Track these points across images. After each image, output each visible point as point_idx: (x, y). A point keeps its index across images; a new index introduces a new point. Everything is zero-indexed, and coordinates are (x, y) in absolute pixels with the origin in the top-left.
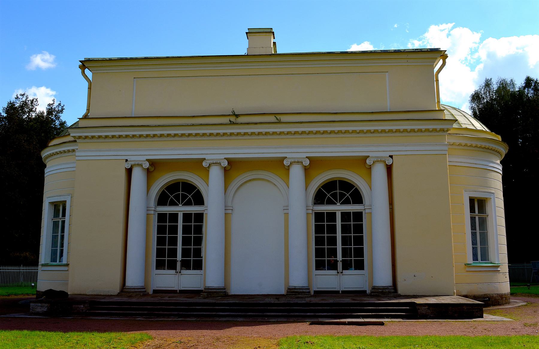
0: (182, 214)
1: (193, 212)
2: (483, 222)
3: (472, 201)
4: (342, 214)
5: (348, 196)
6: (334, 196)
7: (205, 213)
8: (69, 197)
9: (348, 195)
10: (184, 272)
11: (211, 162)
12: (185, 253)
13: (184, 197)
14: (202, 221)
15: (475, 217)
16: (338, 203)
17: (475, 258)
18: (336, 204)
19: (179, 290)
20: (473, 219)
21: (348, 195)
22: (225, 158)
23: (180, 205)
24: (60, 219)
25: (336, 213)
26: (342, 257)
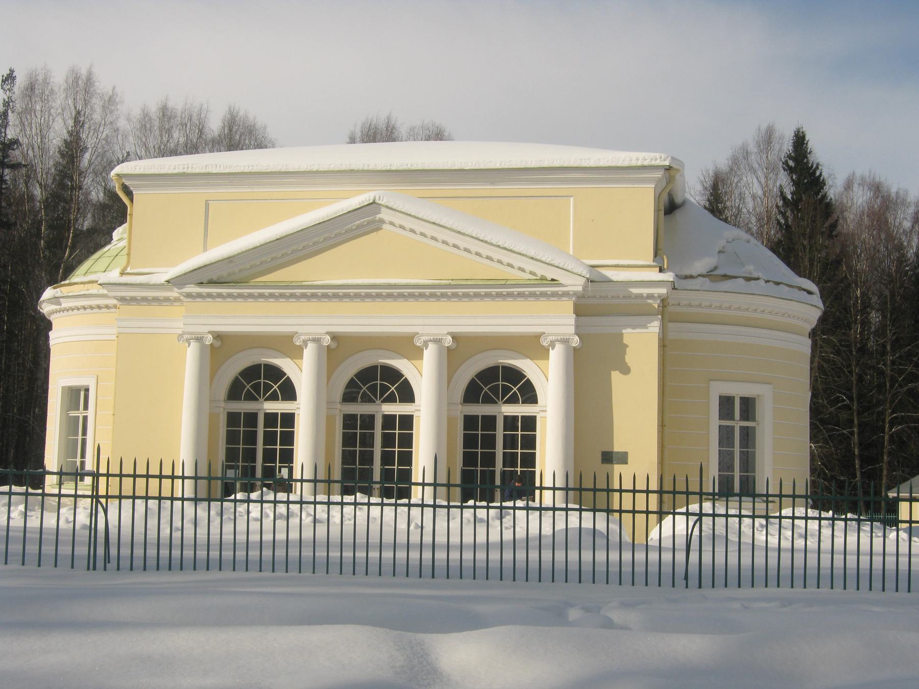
0: (754, 426)
3: (726, 403)
5: (275, 389)
6: (373, 389)
7: (296, 412)
9: (500, 383)
13: (506, 390)
14: (411, 427)
16: (260, 398)
18: (374, 402)
20: (726, 435)
21: (486, 389)
25: (535, 417)
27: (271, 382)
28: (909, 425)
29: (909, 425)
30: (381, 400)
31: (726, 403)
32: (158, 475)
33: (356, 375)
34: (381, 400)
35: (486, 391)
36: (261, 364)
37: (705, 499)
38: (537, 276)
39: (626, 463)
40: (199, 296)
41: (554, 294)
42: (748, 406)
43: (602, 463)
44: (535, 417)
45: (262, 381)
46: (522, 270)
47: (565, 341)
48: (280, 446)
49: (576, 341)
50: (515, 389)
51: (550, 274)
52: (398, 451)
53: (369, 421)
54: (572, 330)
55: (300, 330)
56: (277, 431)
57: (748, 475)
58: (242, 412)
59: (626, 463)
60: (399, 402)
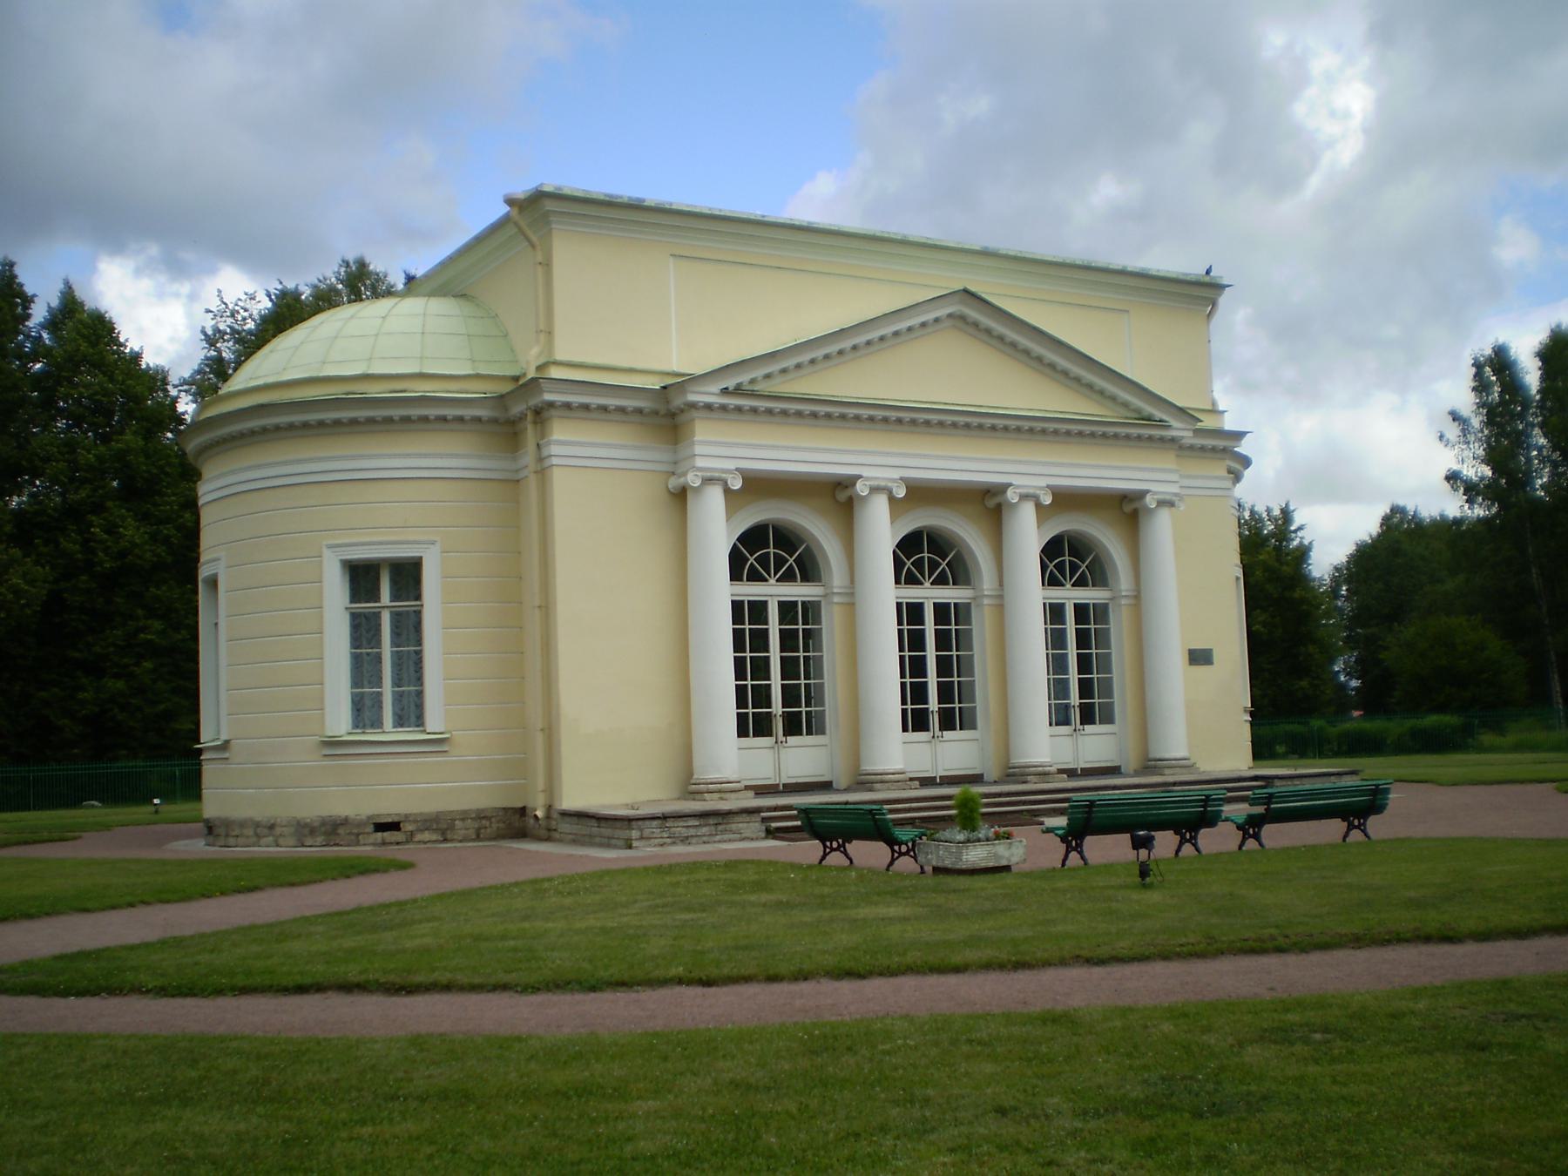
2: (410, 628)
3: (362, 577)
4: (781, 604)
6: (763, 560)
9: (926, 555)
11: (1160, 497)
15: (377, 616)
17: (364, 711)
19: (1081, 769)
20: (363, 629)
23: (772, 581)
25: (766, 602)
30: (931, 581)
31: (362, 577)
34: (777, 576)
40: (723, 408)
41: (1162, 439)
42: (407, 575)
46: (1125, 405)
50: (791, 561)
51: (1158, 414)
52: (909, 651)
55: (865, 472)
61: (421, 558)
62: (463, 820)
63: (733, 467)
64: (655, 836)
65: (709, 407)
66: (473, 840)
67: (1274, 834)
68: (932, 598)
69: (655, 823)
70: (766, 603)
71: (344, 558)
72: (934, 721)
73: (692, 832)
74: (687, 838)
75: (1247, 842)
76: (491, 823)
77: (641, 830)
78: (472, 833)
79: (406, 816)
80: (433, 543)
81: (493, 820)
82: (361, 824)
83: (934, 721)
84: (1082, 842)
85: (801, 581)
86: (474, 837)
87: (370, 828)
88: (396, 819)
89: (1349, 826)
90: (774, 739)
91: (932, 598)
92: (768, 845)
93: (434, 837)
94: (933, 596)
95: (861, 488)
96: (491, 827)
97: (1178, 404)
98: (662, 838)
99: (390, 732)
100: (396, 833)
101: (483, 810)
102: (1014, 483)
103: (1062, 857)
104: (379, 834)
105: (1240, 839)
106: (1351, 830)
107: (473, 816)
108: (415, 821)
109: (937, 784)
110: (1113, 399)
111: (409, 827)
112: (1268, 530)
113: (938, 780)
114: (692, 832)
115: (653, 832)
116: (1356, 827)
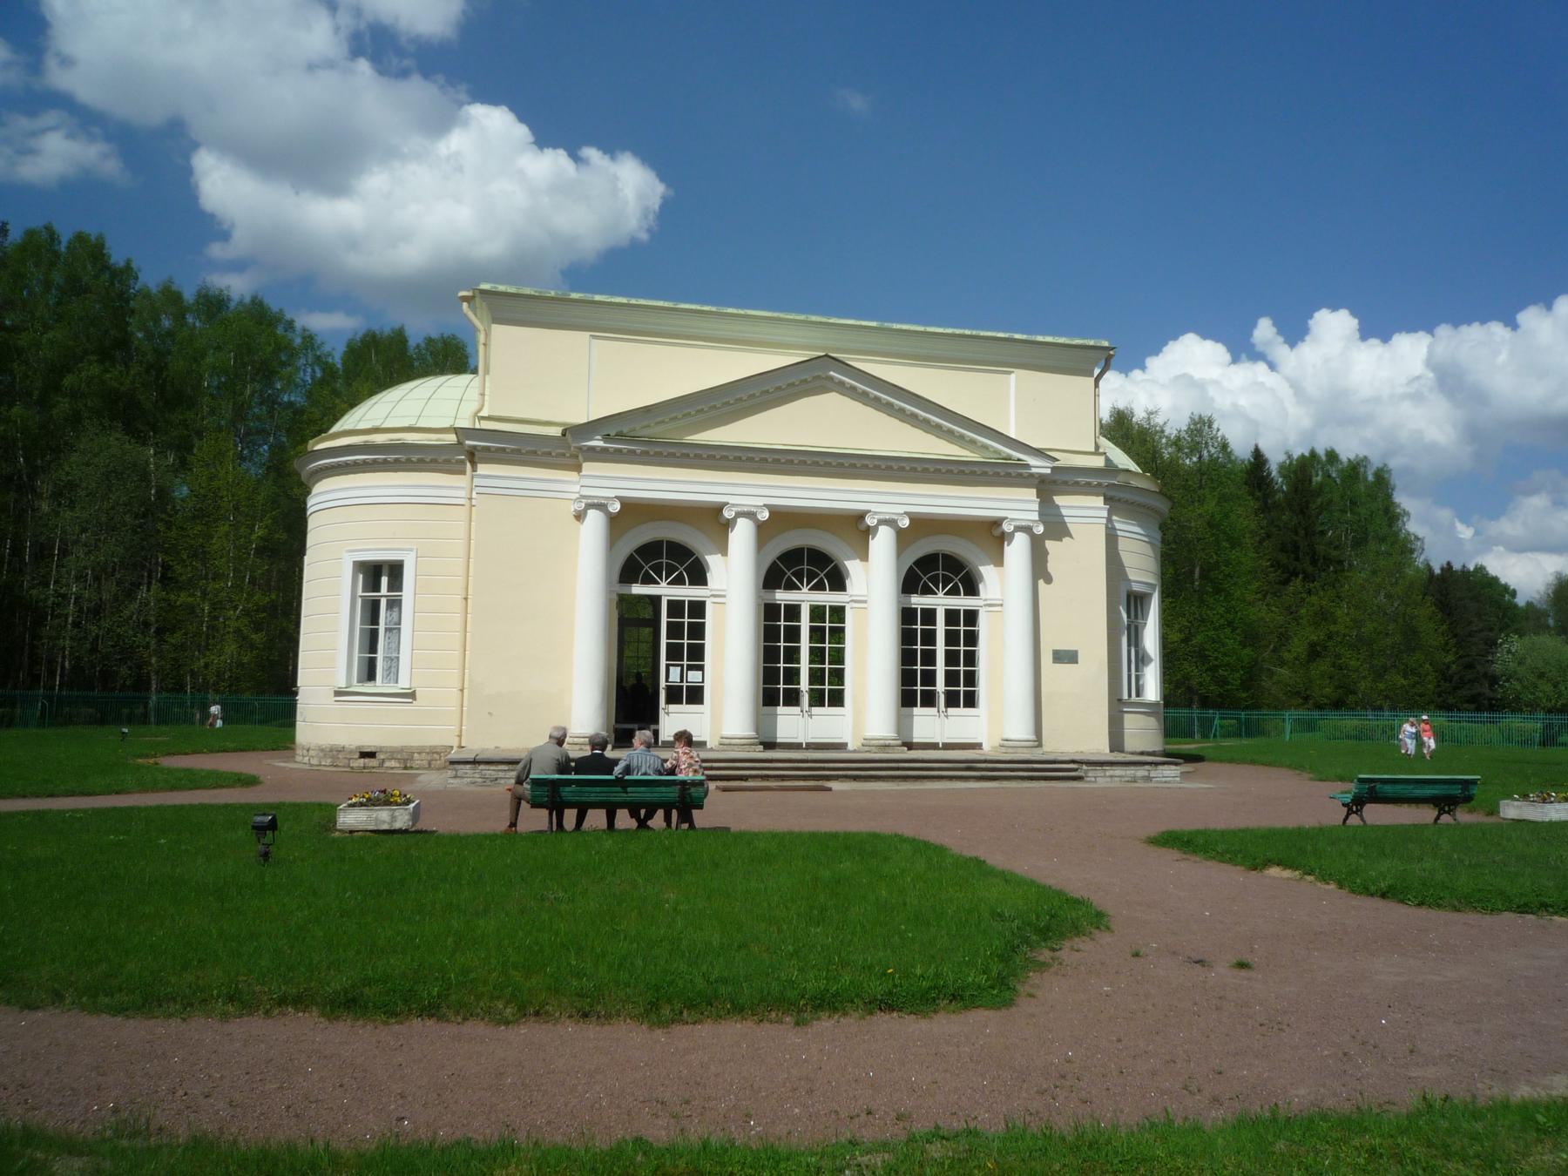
1: (687, 599)
8: (413, 554)
10: (951, 711)
11: (1018, 523)
12: (951, 678)
22: (905, 513)
23: (664, 584)
24: (382, 596)
25: (935, 609)
26: (946, 686)
27: (795, 566)
28: (71, 612)
29: (71, 612)
30: (809, 587)
32: (568, 808)
33: (779, 558)
34: (809, 587)
35: (939, 574)
36: (663, 541)
37: (1138, 695)
38: (1000, 454)
39: (1077, 663)
40: (605, 450)
43: (1054, 662)
44: (935, 609)
45: (681, 569)
47: (1027, 530)
48: (960, 691)
49: (1163, 506)
53: (793, 611)
54: (1035, 516)
55: (731, 500)
56: (687, 661)
57: (370, 653)
58: (901, 626)
59: (1077, 663)
60: (684, 601)
61: (402, 561)
62: (419, 753)
63: (762, 504)
64: (468, 775)
65: (592, 449)
66: (425, 769)
67: (1375, 814)
68: (808, 601)
69: (468, 766)
70: (799, 606)
71: (355, 560)
72: (805, 699)
73: (501, 774)
74: (496, 779)
75: (1442, 817)
76: (440, 757)
77: (456, 770)
78: (425, 763)
79: (381, 748)
80: (411, 550)
81: (442, 754)
82: (351, 752)
83: (805, 699)
84: (1362, 809)
85: (830, 590)
86: (427, 766)
87: (357, 755)
88: (374, 750)
89: (1348, 811)
90: (936, 709)
91: (808, 601)
92: (937, 787)
93: (398, 765)
94: (943, 603)
95: (870, 521)
96: (440, 759)
97: (1034, 446)
98: (473, 777)
99: (380, 685)
100: (372, 760)
101: (435, 747)
102: (730, 502)
103: (1344, 817)
104: (362, 760)
105: (1345, 814)
106: (1442, 814)
107: (427, 751)
108: (386, 752)
109: (803, 749)
110: (973, 442)
111: (381, 756)
112: (154, 496)
113: (804, 746)
114: (501, 774)
115: (466, 773)
116: (1354, 812)
